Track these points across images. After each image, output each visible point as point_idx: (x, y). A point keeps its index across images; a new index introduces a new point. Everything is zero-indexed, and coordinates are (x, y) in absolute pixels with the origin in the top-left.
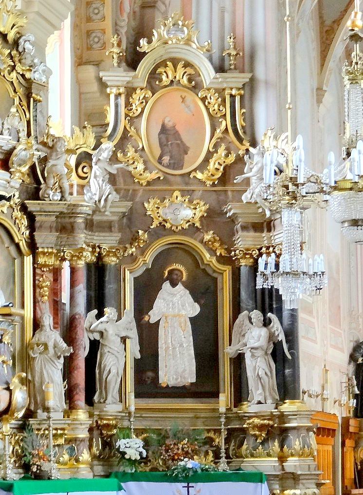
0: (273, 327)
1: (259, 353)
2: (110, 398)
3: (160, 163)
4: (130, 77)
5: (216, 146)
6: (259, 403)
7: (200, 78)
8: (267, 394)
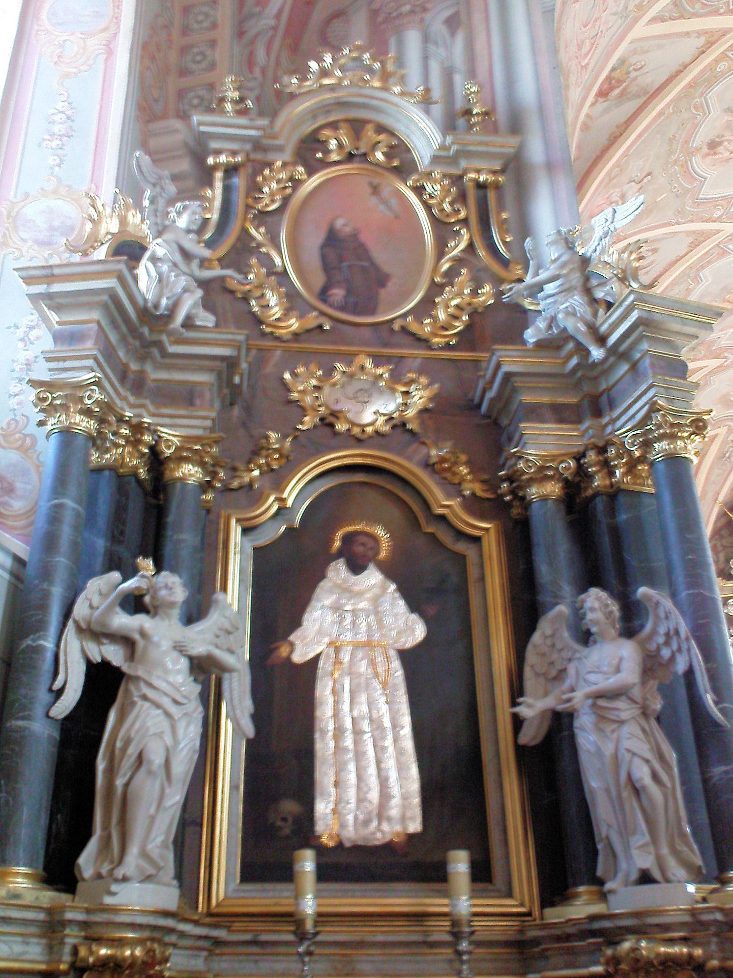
0: (654, 632)
1: (625, 709)
2: (132, 863)
3: (325, 301)
4: (257, 128)
5: (451, 274)
6: (645, 878)
7: (409, 156)
8: (665, 851)
